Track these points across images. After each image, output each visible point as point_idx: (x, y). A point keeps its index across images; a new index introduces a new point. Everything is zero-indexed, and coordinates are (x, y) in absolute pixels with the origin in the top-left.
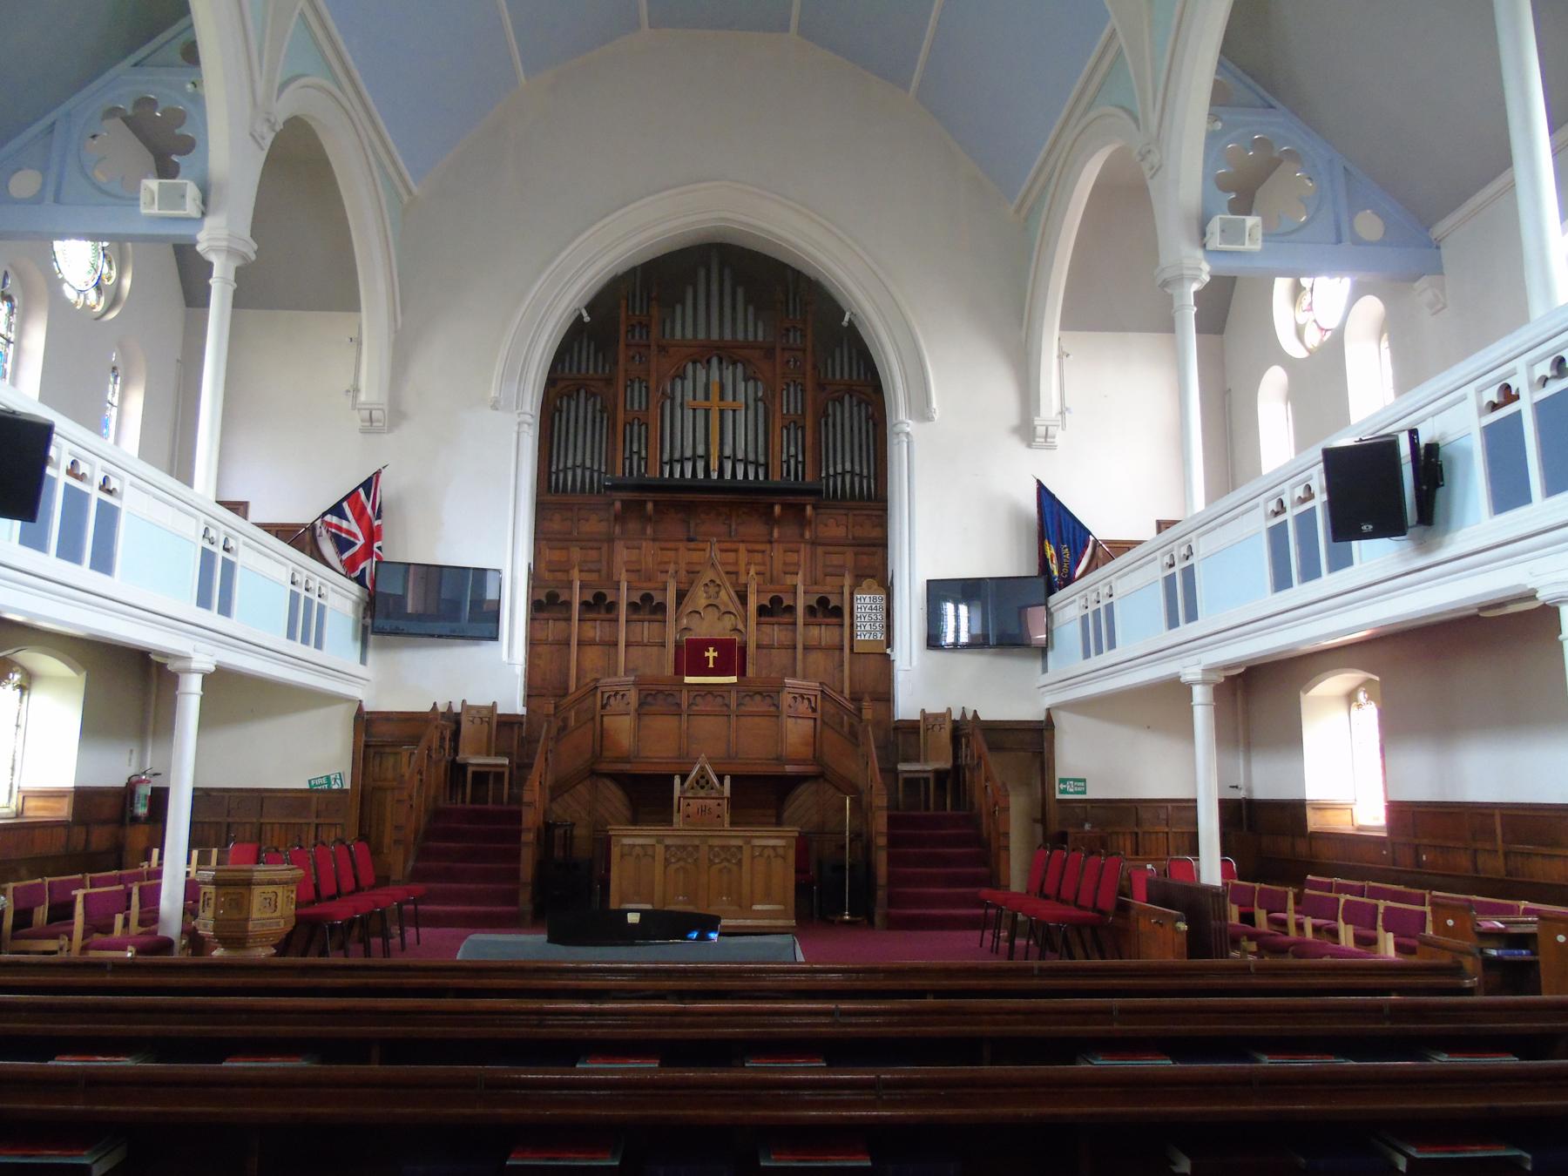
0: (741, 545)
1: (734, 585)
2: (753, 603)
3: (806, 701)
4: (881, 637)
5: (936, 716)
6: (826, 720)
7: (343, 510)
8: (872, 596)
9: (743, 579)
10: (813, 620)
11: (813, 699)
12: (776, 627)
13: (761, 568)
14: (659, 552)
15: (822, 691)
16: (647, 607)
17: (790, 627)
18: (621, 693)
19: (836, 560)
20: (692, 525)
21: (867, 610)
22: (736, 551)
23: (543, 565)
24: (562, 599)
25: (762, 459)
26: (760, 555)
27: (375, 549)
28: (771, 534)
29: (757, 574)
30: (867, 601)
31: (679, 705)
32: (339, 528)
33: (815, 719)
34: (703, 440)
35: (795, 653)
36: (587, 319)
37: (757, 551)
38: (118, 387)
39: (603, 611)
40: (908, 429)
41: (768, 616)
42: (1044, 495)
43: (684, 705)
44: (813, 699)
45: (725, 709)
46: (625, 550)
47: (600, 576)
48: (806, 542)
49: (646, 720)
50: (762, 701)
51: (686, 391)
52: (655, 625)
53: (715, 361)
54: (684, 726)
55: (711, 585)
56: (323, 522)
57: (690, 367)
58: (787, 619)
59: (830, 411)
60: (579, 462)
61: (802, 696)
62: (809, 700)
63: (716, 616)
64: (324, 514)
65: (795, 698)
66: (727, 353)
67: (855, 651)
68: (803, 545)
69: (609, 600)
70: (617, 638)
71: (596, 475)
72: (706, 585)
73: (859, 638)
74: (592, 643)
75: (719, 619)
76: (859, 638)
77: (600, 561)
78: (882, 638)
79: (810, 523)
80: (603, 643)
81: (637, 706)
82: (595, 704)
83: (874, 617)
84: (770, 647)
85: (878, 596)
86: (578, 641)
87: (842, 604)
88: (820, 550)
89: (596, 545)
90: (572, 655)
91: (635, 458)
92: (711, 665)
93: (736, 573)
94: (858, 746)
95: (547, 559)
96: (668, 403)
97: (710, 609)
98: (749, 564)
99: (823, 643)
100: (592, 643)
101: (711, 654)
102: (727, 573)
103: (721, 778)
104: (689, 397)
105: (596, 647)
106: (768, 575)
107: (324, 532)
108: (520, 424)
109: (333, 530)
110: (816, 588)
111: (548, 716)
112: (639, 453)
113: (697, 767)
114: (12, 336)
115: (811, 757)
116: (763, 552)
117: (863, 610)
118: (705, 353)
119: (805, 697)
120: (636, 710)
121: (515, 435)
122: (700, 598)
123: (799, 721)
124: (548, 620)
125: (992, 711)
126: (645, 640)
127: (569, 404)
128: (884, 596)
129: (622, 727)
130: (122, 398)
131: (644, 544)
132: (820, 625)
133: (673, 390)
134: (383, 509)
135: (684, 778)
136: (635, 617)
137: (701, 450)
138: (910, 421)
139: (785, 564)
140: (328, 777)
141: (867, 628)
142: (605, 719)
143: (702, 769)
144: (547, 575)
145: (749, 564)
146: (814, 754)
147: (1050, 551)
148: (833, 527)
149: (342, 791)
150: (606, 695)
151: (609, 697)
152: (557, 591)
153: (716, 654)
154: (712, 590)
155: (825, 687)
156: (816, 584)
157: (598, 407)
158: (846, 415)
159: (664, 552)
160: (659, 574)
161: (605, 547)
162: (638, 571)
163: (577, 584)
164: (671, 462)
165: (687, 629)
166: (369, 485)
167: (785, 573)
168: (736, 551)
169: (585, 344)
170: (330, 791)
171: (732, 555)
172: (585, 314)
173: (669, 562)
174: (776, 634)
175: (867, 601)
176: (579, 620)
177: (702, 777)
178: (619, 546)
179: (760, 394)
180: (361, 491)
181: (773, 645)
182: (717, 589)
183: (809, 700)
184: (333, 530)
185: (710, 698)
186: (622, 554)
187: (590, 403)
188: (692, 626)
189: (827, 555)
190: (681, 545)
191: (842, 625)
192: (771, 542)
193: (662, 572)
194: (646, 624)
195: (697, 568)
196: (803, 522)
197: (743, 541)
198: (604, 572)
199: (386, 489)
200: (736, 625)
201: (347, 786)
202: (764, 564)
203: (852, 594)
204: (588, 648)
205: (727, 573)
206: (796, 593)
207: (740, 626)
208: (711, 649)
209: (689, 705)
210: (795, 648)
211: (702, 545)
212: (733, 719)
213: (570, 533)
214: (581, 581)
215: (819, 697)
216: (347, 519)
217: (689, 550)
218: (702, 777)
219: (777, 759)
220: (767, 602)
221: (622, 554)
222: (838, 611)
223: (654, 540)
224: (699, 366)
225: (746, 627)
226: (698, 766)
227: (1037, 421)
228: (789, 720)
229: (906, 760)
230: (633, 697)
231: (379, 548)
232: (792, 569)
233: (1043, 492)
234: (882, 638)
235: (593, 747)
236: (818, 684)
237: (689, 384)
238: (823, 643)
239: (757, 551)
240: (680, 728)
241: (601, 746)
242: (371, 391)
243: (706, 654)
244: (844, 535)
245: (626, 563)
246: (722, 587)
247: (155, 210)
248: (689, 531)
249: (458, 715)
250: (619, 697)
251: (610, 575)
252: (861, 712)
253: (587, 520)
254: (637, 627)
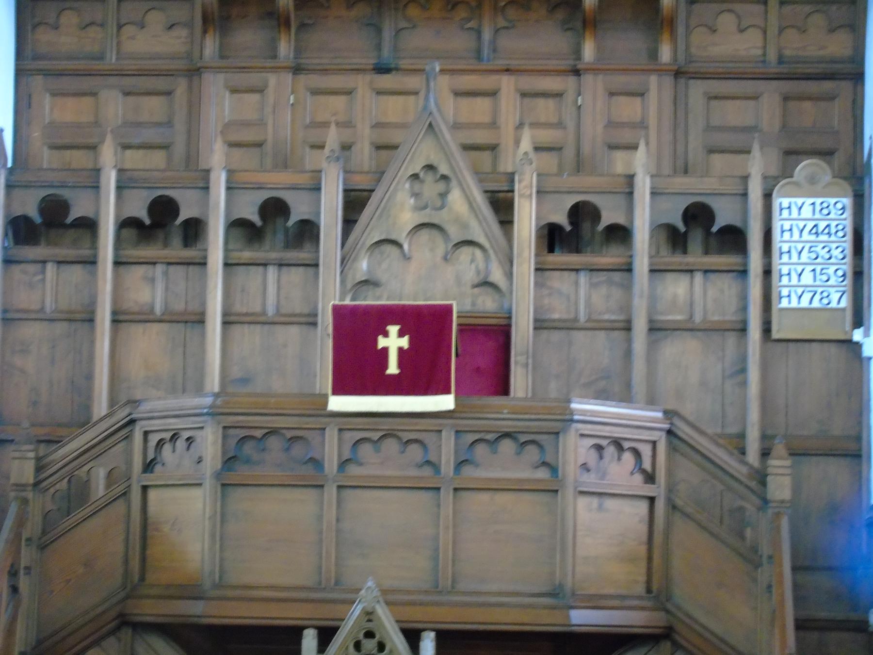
1: (480, 175)
3: (628, 457)
6: (679, 502)
8: (819, 201)
9: (506, 165)
10: (678, 259)
11: (646, 451)
12: (583, 278)
13: (547, 136)
14: (309, 99)
15: (670, 432)
17: (617, 276)
18: (186, 435)
20: (387, 34)
21: (806, 236)
22: (493, 94)
23: (36, 134)
24: (75, 213)
26: (551, 103)
28: (578, 54)
29: (537, 149)
30: (807, 212)
31: (316, 463)
33: (652, 500)
35: (629, 341)
37: (545, 95)
39: (177, 240)
41: (571, 251)
43: (331, 465)
44: (646, 451)
45: (427, 471)
46: (227, 94)
47: (169, 159)
48: (660, 71)
49: (241, 500)
50: (518, 453)
52: (295, 275)
54: (331, 514)
55: (429, 178)
58: (611, 257)
61: (617, 443)
62: (637, 453)
63: (441, 250)
65: (599, 448)
67: (775, 335)
68: (653, 79)
69: (185, 214)
70: (203, 304)
72: (415, 177)
73: (784, 303)
74: (145, 317)
75: (445, 259)
76: (784, 303)
77: (169, 124)
78: (844, 304)
79: (671, 23)
80: (170, 318)
81: (219, 466)
82: (129, 463)
83: (823, 253)
84: (569, 326)
85: (832, 201)
86: (114, 313)
87: (745, 220)
88: (697, 90)
89: (160, 83)
90: (98, 344)
92: (393, 368)
93: (493, 148)
94: (757, 565)
95: (451, 120)
97: (425, 235)
98: (520, 126)
99: (698, 318)
100: (145, 317)
102: (468, 148)
103: (413, 637)
105: (156, 327)
106: (569, 153)
110: (681, 183)
111: (20, 487)
113: (357, 610)
115: (640, 589)
116: (559, 95)
117: (796, 236)
119: (626, 445)
120: (218, 475)
123: (610, 503)
124: (44, 262)
126: (271, 311)
128: (847, 201)
131: (272, 79)
132: (691, 271)
135: (326, 635)
136: (247, 255)
139: (611, 124)
142: (152, 494)
143: (369, 615)
144: (47, 158)
145: (520, 126)
146: (649, 582)
150: (154, 439)
151: (160, 443)
152: (65, 193)
153: (404, 342)
154: (430, 188)
155: (677, 422)
156: (686, 172)
159: (322, 99)
160: (308, 149)
161: (181, 86)
162: (259, 145)
163: (110, 179)
165: (368, 283)
168: (493, 94)
173: (325, 125)
175: (807, 212)
176: (117, 263)
177: (369, 635)
181: (576, 320)
182: (441, 187)
183: (637, 453)
185: (391, 446)
188: (381, 275)
189: (714, 103)
190: (362, 84)
191: (743, 273)
192: (576, 72)
193: (313, 147)
194: (272, 271)
195: (395, 137)
198: (179, 149)
200: (488, 273)
202: (560, 125)
203: (768, 197)
204: (137, 330)
205: (468, 148)
206: (631, 194)
207: (497, 276)
208: (393, 330)
209: (343, 464)
210: (627, 327)
211: (413, 82)
212: (447, 496)
213: (101, 57)
214: (121, 171)
215: (662, 448)
217: (380, 93)
218: (369, 635)
219: (552, 595)
220: (561, 218)
223: (297, 70)
225: (509, 275)
226: (360, 607)
228: (582, 501)
232: (626, 136)
234: (844, 304)
235: (126, 561)
236: (660, 415)
238: (698, 318)
239: (545, 95)
240: (320, 518)
241: (143, 559)
243: (382, 342)
244: (759, 52)
245: (227, 127)
246: (454, 183)
248: (379, 47)
250: (181, 444)
251: (191, 159)
252: (763, 483)
253: (142, 26)
254: (251, 278)
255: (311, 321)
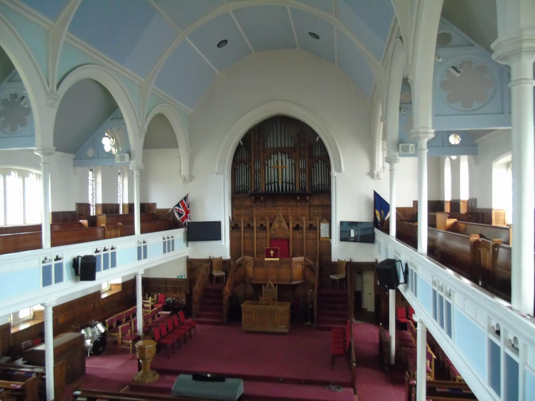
0: (288, 208)
2: (291, 226)
4: (328, 236)
5: (342, 262)
7: (179, 205)
16: (262, 228)
19: (316, 211)
25: (294, 182)
27: (188, 216)
30: (324, 225)
32: (179, 210)
34: (277, 178)
36: (242, 144)
37: (293, 209)
38: (121, 178)
40: (335, 175)
42: (376, 195)
51: (271, 163)
53: (279, 154)
56: (175, 208)
57: (272, 156)
59: (315, 165)
60: (243, 184)
61: (298, 262)
64: (175, 206)
66: (283, 150)
71: (248, 188)
72: (278, 222)
91: (258, 183)
92: (272, 255)
96: (266, 167)
101: (272, 252)
104: (272, 165)
107: (175, 211)
108: (224, 178)
109: (178, 211)
112: (259, 182)
114: (94, 179)
118: (276, 151)
121: (223, 182)
122: (276, 225)
125: (358, 259)
127: (239, 167)
128: (328, 224)
129: (250, 269)
130: (123, 181)
133: (268, 162)
134: (190, 204)
135: (265, 286)
137: (276, 180)
138: (336, 173)
140: (181, 276)
141: (324, 234)
147: (377, 212)
148: (316, 201)
149: (185, 279)
157: (248, 168)
158: (319, 166)
164: (268, 184)
166: (185, 198)
167: (302, 216)
168: (287, 209)
169: (243, 149)
170: (182, 279)
171: (286, 211)
172: (241, 142)
174: (298, 235)
178: (254, 209)
179: (293, 163)
180: (184, 200)
184: (178, 211)
186: (255, 211)
187: (245, 166)
191: (316, 233)
194: (262, 233)
196: (306, 201)
197: (289, 207)
199: (190, 198)
201: (186, 278)
216: (181, 208)
220: (295, 226)
221: (255, 211)
222: (315, 229)
223: (264, 207)
224: (275, 155)
227: (374, 172)
229: (333, 274)
230: (252, 263)
231: (189, 216)
233: (376, 194)
237: (272, 160)
239: (293, 209)
242: (185, 172)
247: (119, 162)
249: (212, 259)
255: (266, 238)
